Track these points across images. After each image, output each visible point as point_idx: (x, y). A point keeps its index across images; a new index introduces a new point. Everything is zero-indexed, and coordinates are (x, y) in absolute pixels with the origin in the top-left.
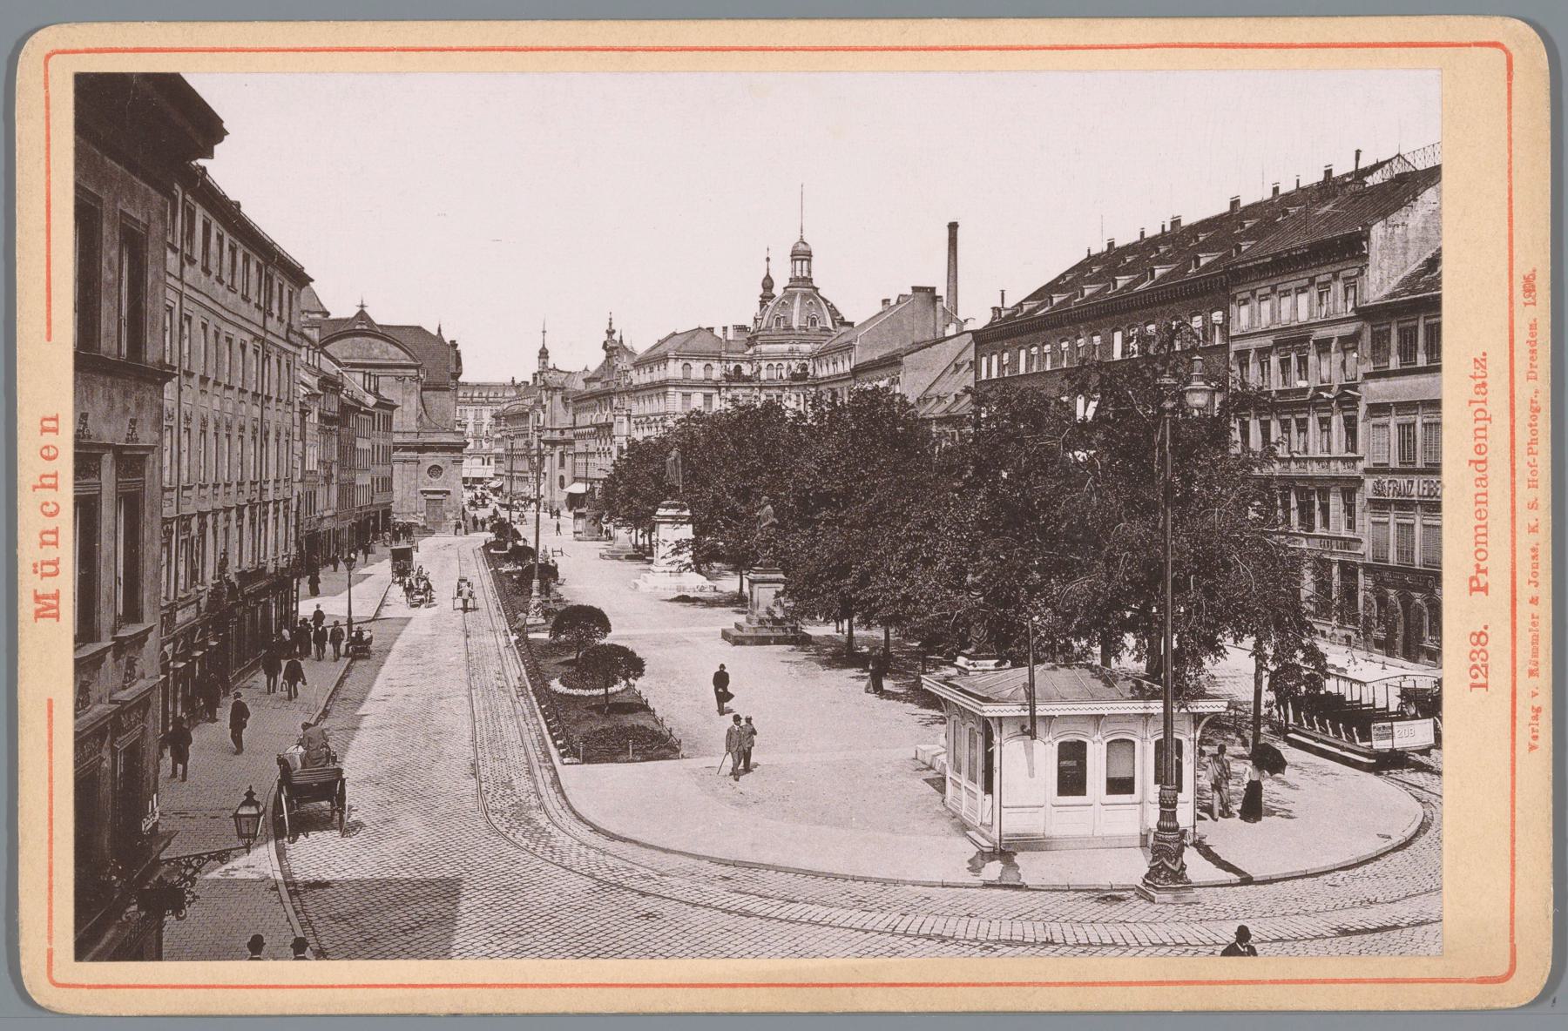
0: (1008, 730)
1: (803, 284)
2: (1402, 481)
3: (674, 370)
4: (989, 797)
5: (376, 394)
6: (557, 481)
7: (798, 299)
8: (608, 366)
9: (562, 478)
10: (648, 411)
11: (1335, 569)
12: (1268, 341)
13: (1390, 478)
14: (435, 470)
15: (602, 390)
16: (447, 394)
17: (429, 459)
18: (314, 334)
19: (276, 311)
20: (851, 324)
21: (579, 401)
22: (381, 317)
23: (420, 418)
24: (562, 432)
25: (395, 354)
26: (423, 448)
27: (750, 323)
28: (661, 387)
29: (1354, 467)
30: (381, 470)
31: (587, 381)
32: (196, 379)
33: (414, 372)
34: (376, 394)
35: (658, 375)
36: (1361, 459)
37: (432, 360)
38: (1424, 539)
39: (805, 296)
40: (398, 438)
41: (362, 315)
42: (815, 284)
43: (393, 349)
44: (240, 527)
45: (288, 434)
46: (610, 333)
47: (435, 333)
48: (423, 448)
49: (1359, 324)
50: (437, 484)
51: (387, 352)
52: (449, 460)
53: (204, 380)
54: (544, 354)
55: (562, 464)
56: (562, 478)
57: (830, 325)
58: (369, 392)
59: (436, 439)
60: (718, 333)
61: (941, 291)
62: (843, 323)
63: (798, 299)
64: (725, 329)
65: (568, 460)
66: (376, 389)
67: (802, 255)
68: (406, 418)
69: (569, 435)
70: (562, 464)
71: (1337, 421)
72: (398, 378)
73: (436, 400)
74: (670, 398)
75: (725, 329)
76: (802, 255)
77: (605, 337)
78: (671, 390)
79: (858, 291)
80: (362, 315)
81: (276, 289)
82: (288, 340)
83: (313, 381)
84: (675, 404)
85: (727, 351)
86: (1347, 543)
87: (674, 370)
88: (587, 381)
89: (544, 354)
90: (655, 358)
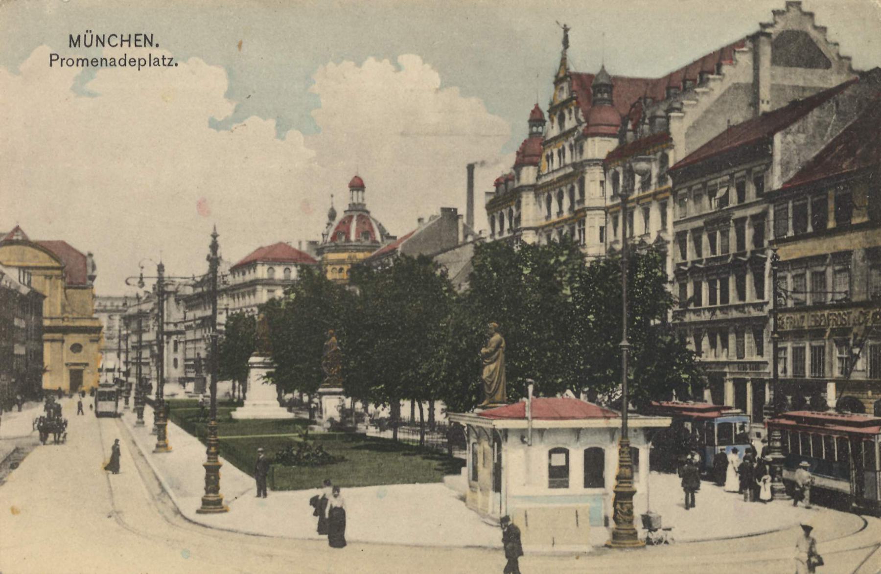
0: (513, 439)
1: (359, 211)
2: (797, 316)
3: (262, 272)
4: (498, 494)
5: (29, 285)
6: (172, 361)
9: (175, 360)
10: (241, 305)
11: (749, 385)
12: (700, 223)
13: (788, 315)
15: (209, 290)
17: (72, 339)
20: (395, 238)
21: (190, 302)
23: (63, 307)
24: (176, 325)
26: (66, 330)
28: (253, 284)
29: (762, 310)
30: (33, 345)
34: (29, 285)
35: (249, 277)
36: (767, 303)
37: (71, 268)
38: (813, 359)
40: (47, 323)
48: (66, 330)
49: (765, 205)
50: (76, 358)
52: (87, 340)
55: (176, 350)
56: (175, 360)
59: (77, 324)
61: (462, 210)
62: (389, 237)
63: (355, 218)
64: (300, 243)
65: (181, 347)
66: (29, 282)
67: (357, 185)
68: (52, 307)
69: (181, 327)
70: (176, 350)
71: (749, 279)
72: (46, 277)
73: (77, 295)
74: (258, 294)
75: (300, 243)
76: (357, 185)
78: (259, 288)
79: (400, 219)
84: (263, 296)
86: (757, 365)
87: (262, 272)
90: (248, 264)
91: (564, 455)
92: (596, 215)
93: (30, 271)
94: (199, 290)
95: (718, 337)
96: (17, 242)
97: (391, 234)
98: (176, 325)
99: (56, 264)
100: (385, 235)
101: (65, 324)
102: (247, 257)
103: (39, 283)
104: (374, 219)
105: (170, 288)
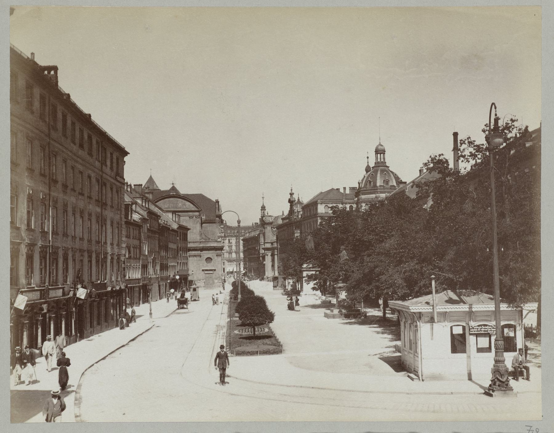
7: (379, 172)
8: (291, 211)
14: (209, 260)
16: (214, 225)
17: (206, 254)
18: (150, 196)
19: (108, 163)
20: (406, 183)
22: (183, 191)
24: (272, 243)
25: (189, 206)
26: (202, 249)
27: (357, 186)
31: (283, 219)
32: (60, 184)
33: (197, 214)
37: (207, 209)
39: (382, 171)
41: (173, 188)
42: (387, 165)
43: (192, 205)
44: (90, 261)
45: (118, 223)
46: (291, 194)
47: (236, 225)
48: (202, 249)
51: (185, 205)
52: (215, 255)
53: (65, 186)
54: (263, 208)
57: (395, 184)
58: (175, 222)
60: (342, 191)
62: (401, 182)
63: (379, 172)
64: (345, 188)
67: (380, 151)
68: (193, 236)
75: (345, 188)
76: (380, 151)
77: (289, 196)
80: (173, 188)
81: (109, 155)
82: (116, 180)
83: (145, 214)
85: (346, 199)
88: (283, 219)
89: (263, 208)
91: (488, 339)
92: (180, 208)
93: (179, 214)
94: (285, 221)
95: (25, 334)
96: (173, 197)
97: (403, 181)
98: (272, 243)
99: (194, 208)
100: (399, 182)
101: (201, 245)
102: (311, 200)
103: (185, 221)
104: (391, 172)
105: (270, 220)
